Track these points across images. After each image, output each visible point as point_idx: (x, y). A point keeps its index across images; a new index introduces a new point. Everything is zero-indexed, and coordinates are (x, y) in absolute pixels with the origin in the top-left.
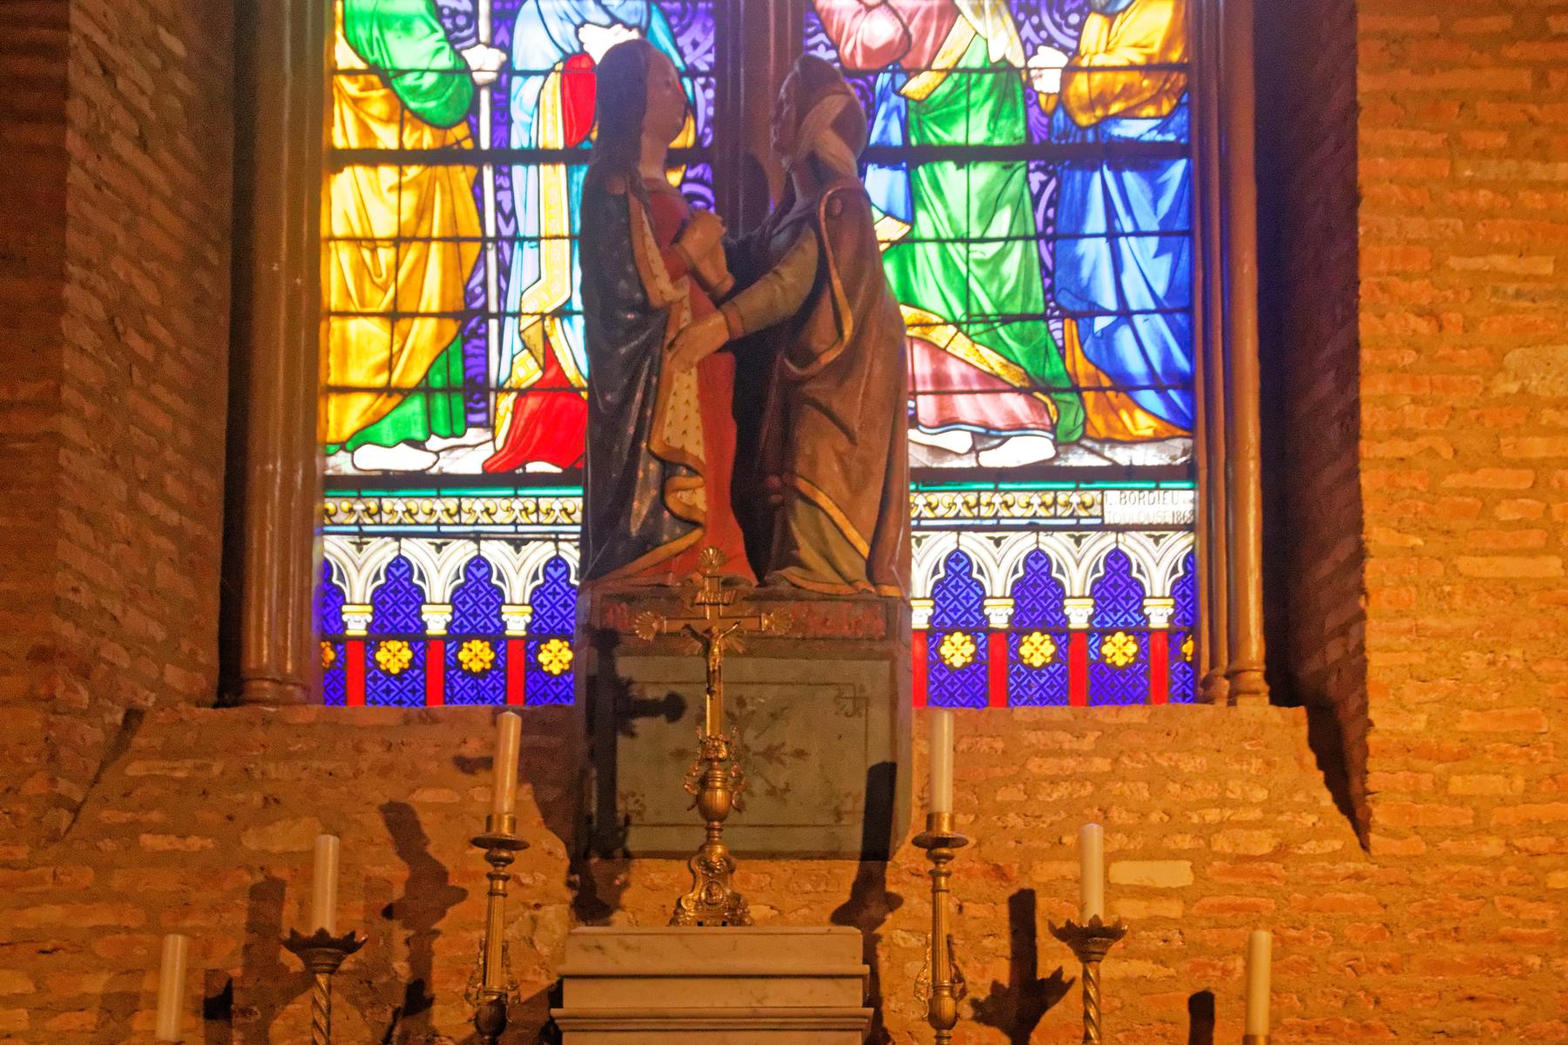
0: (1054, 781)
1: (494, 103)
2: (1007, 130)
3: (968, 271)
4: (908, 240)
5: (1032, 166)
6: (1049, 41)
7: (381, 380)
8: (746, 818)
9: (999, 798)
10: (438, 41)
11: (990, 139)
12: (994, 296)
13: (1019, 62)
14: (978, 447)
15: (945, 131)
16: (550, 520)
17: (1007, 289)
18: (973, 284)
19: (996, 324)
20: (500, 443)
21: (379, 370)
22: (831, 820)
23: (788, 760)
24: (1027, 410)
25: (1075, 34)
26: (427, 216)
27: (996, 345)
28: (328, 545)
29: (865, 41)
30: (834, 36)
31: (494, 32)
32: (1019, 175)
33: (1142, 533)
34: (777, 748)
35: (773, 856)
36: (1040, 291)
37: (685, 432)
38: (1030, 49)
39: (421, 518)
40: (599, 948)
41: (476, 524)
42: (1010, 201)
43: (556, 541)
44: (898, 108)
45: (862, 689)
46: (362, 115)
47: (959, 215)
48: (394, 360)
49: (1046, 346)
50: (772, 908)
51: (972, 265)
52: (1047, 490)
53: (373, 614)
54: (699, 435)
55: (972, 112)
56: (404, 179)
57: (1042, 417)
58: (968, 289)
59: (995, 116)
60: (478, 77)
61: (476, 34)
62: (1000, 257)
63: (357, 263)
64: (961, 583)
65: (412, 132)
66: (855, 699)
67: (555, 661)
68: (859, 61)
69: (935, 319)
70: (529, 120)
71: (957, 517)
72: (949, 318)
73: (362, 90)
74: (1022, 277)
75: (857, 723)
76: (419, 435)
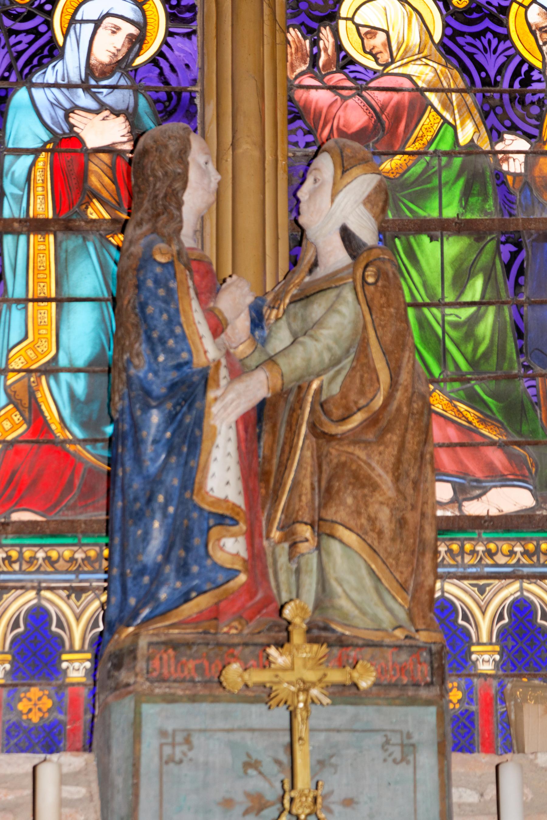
2: (478, 206)
6: (513, 129)
12: (469, 356)
14: (461, 498)
16: (33, 569)
17: (482, 349)
18: (449, 344)
19: (473, 382)
23: (337, 808)
25: (537, 123)
29: (341, 126)
30: (312, 125)
32: (490, 247)
33: (466, 582)
36: (514, 350)
42: (482, 270)
43: (39, 590)
45: (409, 736)
47: (434, 278)
49: (522, 402)
51: (447, 327)
52: (531, 539)
53: (501, 653)
58: (445, 350)
59: (466, 194)
62: (474, 320)
66: (402, 745)
67: (35, 710)
70: (19, 192)
74: (496, 339)
75: (405, 770)
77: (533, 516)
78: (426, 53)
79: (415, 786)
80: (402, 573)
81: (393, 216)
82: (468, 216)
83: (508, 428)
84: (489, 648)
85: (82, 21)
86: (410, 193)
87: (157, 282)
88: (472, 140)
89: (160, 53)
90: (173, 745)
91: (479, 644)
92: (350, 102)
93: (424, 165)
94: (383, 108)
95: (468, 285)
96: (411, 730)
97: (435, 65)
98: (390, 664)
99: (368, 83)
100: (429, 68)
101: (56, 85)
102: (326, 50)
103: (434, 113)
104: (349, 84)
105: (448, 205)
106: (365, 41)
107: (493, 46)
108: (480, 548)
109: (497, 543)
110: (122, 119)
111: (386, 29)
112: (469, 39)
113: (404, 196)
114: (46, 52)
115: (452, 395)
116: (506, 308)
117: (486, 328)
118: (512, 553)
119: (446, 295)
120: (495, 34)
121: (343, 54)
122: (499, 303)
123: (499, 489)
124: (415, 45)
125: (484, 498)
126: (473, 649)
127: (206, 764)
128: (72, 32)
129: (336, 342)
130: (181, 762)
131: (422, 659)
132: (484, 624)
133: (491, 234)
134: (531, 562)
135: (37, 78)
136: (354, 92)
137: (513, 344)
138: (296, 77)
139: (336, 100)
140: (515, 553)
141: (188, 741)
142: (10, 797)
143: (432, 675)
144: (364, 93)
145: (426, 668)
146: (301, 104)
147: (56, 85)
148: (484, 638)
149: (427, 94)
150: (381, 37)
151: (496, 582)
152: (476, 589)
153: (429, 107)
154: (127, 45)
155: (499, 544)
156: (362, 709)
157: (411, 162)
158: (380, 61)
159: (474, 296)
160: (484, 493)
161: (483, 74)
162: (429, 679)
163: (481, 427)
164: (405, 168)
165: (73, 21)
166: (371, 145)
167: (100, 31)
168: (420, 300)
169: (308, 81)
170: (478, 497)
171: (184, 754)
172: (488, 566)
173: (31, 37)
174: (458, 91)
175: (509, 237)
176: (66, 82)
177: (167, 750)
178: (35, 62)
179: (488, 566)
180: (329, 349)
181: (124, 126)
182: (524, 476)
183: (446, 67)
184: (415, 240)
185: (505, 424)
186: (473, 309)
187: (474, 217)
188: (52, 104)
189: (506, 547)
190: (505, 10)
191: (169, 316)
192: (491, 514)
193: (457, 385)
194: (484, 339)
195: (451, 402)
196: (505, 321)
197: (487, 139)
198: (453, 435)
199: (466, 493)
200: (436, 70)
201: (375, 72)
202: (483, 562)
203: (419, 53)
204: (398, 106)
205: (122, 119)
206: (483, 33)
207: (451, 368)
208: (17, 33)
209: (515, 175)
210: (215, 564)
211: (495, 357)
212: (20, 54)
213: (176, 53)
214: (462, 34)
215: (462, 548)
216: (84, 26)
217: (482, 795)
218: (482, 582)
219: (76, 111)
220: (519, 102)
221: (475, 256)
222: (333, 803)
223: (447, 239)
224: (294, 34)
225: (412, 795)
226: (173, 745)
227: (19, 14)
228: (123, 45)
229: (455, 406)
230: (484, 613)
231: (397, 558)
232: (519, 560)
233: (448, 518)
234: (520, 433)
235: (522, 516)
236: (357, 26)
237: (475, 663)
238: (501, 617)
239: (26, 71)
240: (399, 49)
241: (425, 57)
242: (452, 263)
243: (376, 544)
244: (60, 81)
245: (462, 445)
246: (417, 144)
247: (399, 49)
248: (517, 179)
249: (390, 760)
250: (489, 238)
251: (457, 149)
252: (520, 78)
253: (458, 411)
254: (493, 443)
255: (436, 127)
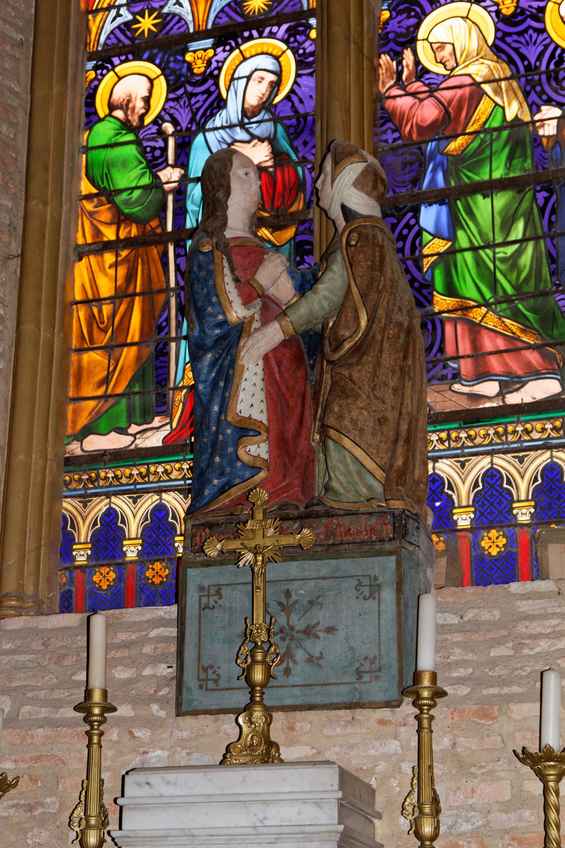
0: (536, 637)
1: (175, 201)
2: (519, 166)
3: (495, 266)
4: (452, 252)
5: (538, 188)
6: (549, 102)
7: (100, 392)
8: (292, 680)
9: (492, 655)
10: (142, 169)
11: (507, 174)
12: (514, 282)
13: (527, 118)
14: (504, 391)
15: (474, 174)
18: (499, 276)
19: (517, 302)
20: (174, 425)
21: (100, 384)
22: (353, 679)
23: (321, 635)
24: (540, 360)
26: (133, 280)
27: (516, 316)
28: (65, 505)
29: (419, 122)
30: (398, 124)
31: (177, 156)
32: (529, 196)
33: (509, 455)
34: (314, 627)
35: (311, 707)
36: (548, 273)
37: (252, 405)
38: (534, 108)
39: (124, 480)
40: (148, 783)
41: (159, 481)
42: (523, 214)
44: (442, 164)
45: (376, 579)
46: (95, 222)
48: (110, 377)
49: (554, 312)
50: (312, 748)
51: (497, 263)
53: (535, 507)
54: (264, 406)
55: (494, 158)
56: (119, 259)
57: (552, 364)
58: (496, 280)
59: (510, 158)
60: (167, 187)
61: (166, 160)
62: (518, 254)
63: (89, 316)
64: (495, 492)
65: (125, 228)
66: (370, 586)
68: (415, 136)
69: (472, 303)
71: (490, 444)
72: (481, 301)
73: (96, 207)
74: (534, 266)
75: (372, 605)
76: (123, 424)
77: (557, 400)
78: (482, 54)
79: (379, 616)
80: (382, 458)
81: (455, 184)
82: (512, 175)
83: (543, 334)
84: (527, 504)
85: (239, 78)
86: (468, 165)
87: (200, 267)
88: (517, 116)
89: (292, 91)
90: (208, 596)
91: (519, 501)
92: (426, 102)
93: (479, 141)
94: (450, 102)
95: (513, 228)
96: (377, 575)
97: (489, 63)
98: (363, 527)
99: (439, 85)
100: (484, 66)
101: (223, 128)
102: (408, 66)
103: (488, 99)
104: (426, 89)
105: (497, 169)
106: (437, 54)
107: (534, 39)
108: (520, 428)
109: (532, 423)
110: (266, 143)
111: (452, 42)
112: (515, 37)
113: (464, 168)
114: (215, 105)
115: (501, 313)
116: (542, 242)
117: (526, 259)
118: (544, 430)
119: (496, 238)
120: (535, 30)
121: (420, 67)
122: (536, 238)
123: (534, 382)
124: (473, 51)
125: (522, 390)
126: (515, 505)
127: (231, 608)
128: (232, 87)
129: (331, 292)
130: (214, 607)
131: (387, 522)
132: (523, 486)
133: (529, 185)
134: (559, 435)
135: (209, 125)
136: (428, 94)
137: (547, 269)
138: (387, 91)
139: (415, 103)
140: (546, 429)
141: (218, 593)
142: (133, 637)
143: (394, 532)
144: (436, 94)
145: (390, 528)
146: (390, 110)
147: (223, 128)
148: (523, 497)
149: (483, 86)
150: (449, 48)
151: (532, 453)
152: (517, 460)
153: (485, 96)
154: (269, 90)
155: (534, 423)
156: (341, 562)
157: (470, 140)
158: (448, 67)
159: (517, 236)
160: (522, 387)
161: (526, 63)
162: (391, 536)
163: (522, 335)
164: (465, 145)
165: (232, 79)
166: (440, 132)
167: (251, 82)
168: (476, 244)
169: (396, 92)
170: (518, 390)
171: (216, 602)
172: (526, 441)
173: (206, 96)
174: (505, 79)
175: (543, 186)
176: (229, 124)
177: (204, 600)
178: (208, 113)
179: (526, 441)
180: (326, 298)
181: (267, 148)
182: (554, 369)
183: (497, 62)
184: (472, 199)
185: (541, 331)
186: (516, 246)
187: (515, 175)
188: (219, 141)
189: (539, 426)
190: (542, 10)
191: (208, 290)
192: (525, 401)
193: (504, 306)
194: (525, 267)
195: (500, 319)
196: (541, 252)
197: (528, 113)
198: (501, 344)
199: (509, 388)
200: (489, 67)
201: (444, 76)
202: (522, 439)
203: (477, 55)
204: (461, 100)
205: (266, 143)
206: (526, 30)
207: (501, 293)
208: (196, 95)
209: (549, 137)
210: (243, 464)
211: (533, 281)
212: (198, 109)
213: (303, 88)
214: (510, 34)
215: (506, 430)
216: (240, 81)
217: (462, 617)
218: (521, 454)
219: (236, 144)
220: (554, 80)
221: (517, 205)
222: (320, 631)
223: (496, 195)
224: (385, 59)
225: (377, 622)
226: (208, 596)
227: (197, 81)
228: (267, 90)
229: (503, 322)
230: (522, 478)
231: (378, 448)
232: (549, 434)
233: (493, 408)
234: (551, 337)
235: (550, 401)
236: (431, 44)
237: (515, 516)
238: (536, 480)
239: (203, 121)
240: (461, 55)
241: (482, 58)
242: (500, 213)
243: (357, 439)
244: (225, 124)
245: (505, 351)
246: (475, 125)
247: (461, 55)
248: (551, 140)
249: (361, 597)
250: (527, 189)
251: (505, 124)
252: (554, 61)
253: (505, 325)
254: (529, 347)
255: (489, 110)
